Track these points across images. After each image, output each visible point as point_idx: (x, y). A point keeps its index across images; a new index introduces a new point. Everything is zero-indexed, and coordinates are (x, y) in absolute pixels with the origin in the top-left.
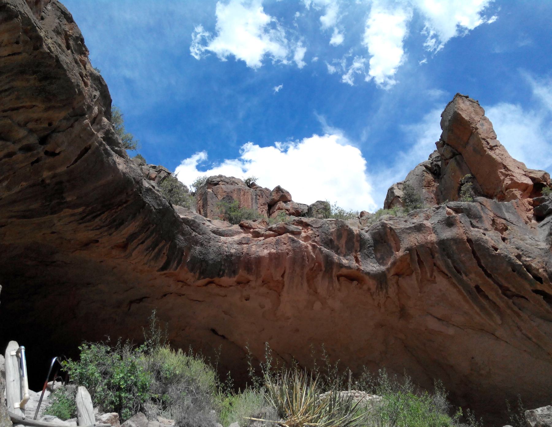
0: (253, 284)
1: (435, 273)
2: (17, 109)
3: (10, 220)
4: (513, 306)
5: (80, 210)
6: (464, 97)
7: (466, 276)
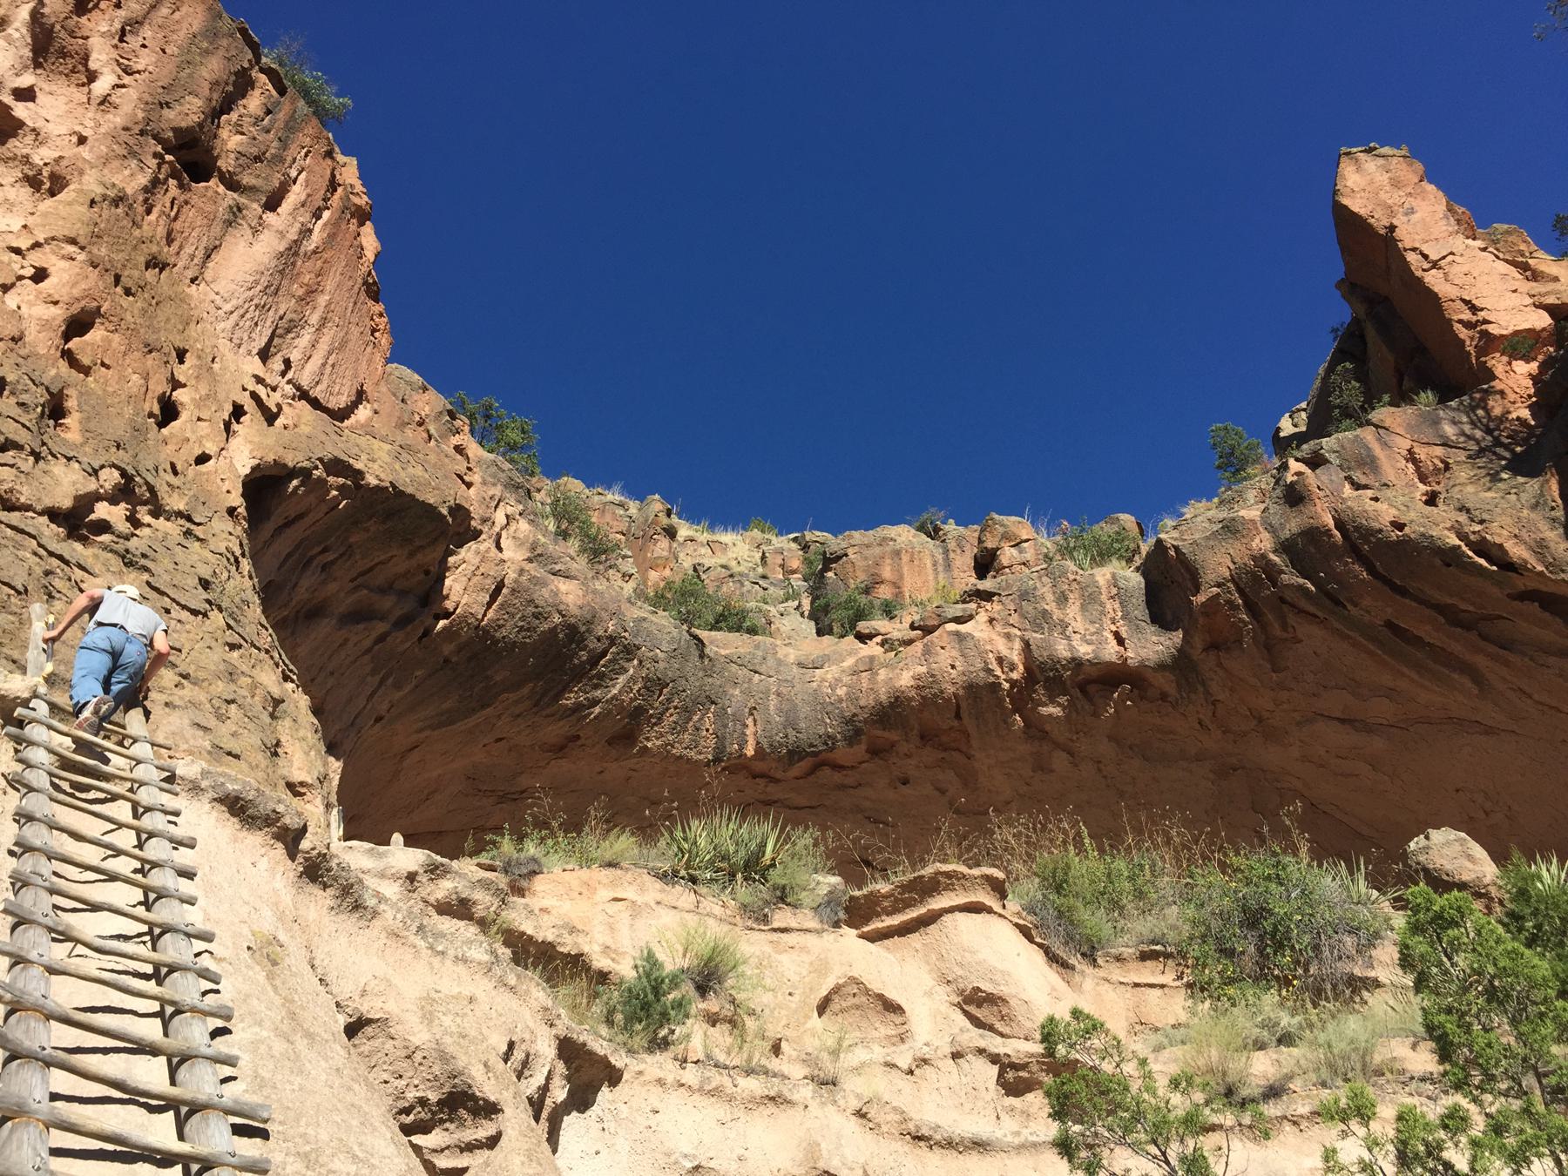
0: (903, 748)
1: (1292, 619)
2: (371, 569)
3: (422, 735)
4: (1482, 644)
5: (525, 691)
6: (178, 707)
7: (1356, 606)
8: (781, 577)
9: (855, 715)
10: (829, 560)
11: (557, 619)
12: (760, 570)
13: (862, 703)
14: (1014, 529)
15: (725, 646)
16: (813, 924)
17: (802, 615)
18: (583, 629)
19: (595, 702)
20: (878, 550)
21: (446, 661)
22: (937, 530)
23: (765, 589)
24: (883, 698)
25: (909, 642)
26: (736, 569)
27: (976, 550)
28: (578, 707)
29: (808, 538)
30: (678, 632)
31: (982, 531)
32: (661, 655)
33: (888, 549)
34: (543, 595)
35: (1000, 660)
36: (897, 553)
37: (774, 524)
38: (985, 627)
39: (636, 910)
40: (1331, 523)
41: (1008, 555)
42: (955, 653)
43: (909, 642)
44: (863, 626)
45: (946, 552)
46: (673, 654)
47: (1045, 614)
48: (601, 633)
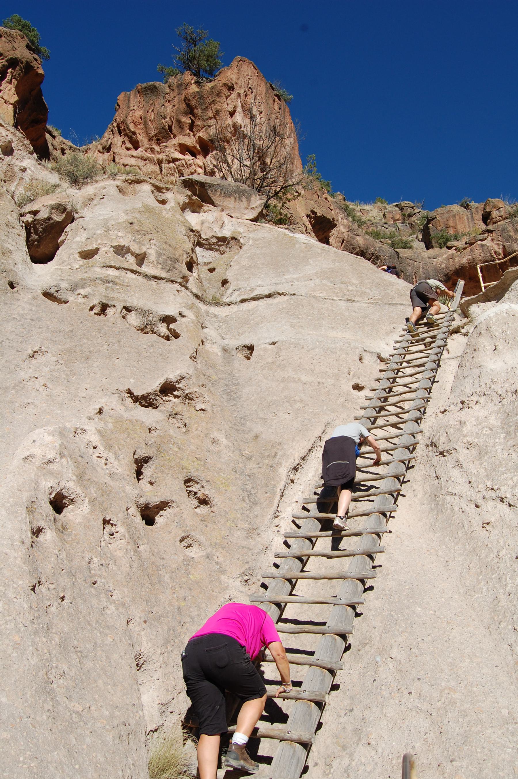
8: (392, 222)
9: (448, 273)
10: (429, 220)
12: (383, 220)
13: (451, 269)
14: (496, 203)
15: (404, 254)
17: (419, 240)
20: (447, 215)
22: (468, 205)
23: (387, 228)
24: (457, 267)
25: (464, 249)
26: (374, 221)
27: (483, 212)
29: (402, 205)
30: (391, 250)
31: (485, 205)
32: (387, 258)
33: (451, 214)
34: (354, 242)
35: (495, 252)
36: (454, 216)
37: (386, 200)
38: (490, 242)
41: (495, 213)
42: (481, 251)
43: (464, 249)
44: (449, 244)
45: (472, 213)
46: (390, 257)
47: (510, 236)
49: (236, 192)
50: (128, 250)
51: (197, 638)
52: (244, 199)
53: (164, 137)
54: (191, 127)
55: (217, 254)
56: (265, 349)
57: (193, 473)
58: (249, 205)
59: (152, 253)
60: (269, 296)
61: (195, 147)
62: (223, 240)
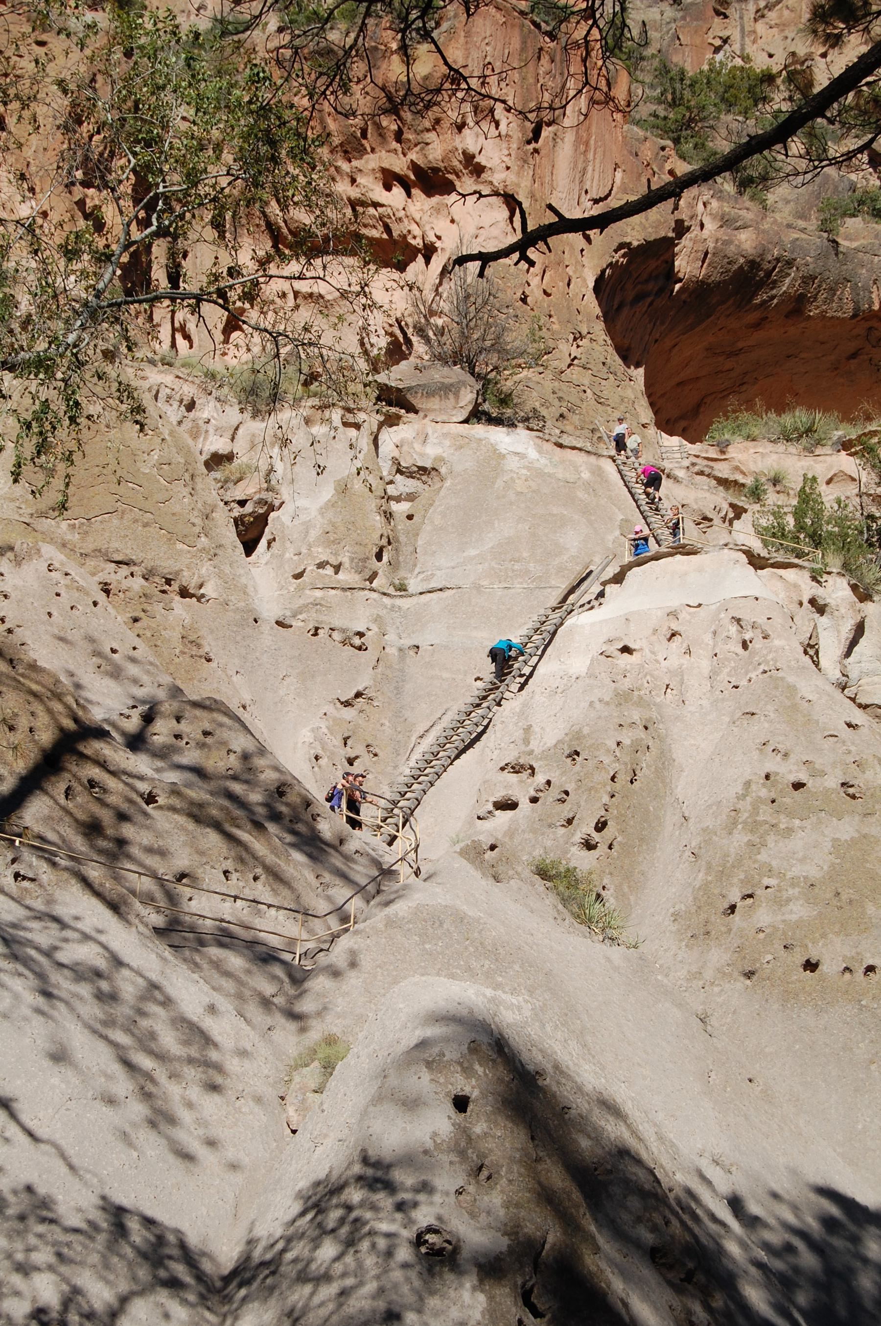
5: (731, 301)
11: (742, 260)
16: (830, 452)
18: (758, 260)
19: (773, 297)
21: (684, 302)
28: (764, 302)
34: (731, 250)
39: (763, 455)
40: (266, 825)
46: (818, 257)
48: (770, 258)
49: (440, 389)
50: (327, 563)
51: (623, 1312)
52: (451, 396)
53: (355, 149)
54: (399, 136)
55: (418, 483)
56: (426, 650)
57: (370, 742)
58: (457, 403)
59: (346, 560)
60: (441, 590)
61: (407, 176)
62: (423, 470)
